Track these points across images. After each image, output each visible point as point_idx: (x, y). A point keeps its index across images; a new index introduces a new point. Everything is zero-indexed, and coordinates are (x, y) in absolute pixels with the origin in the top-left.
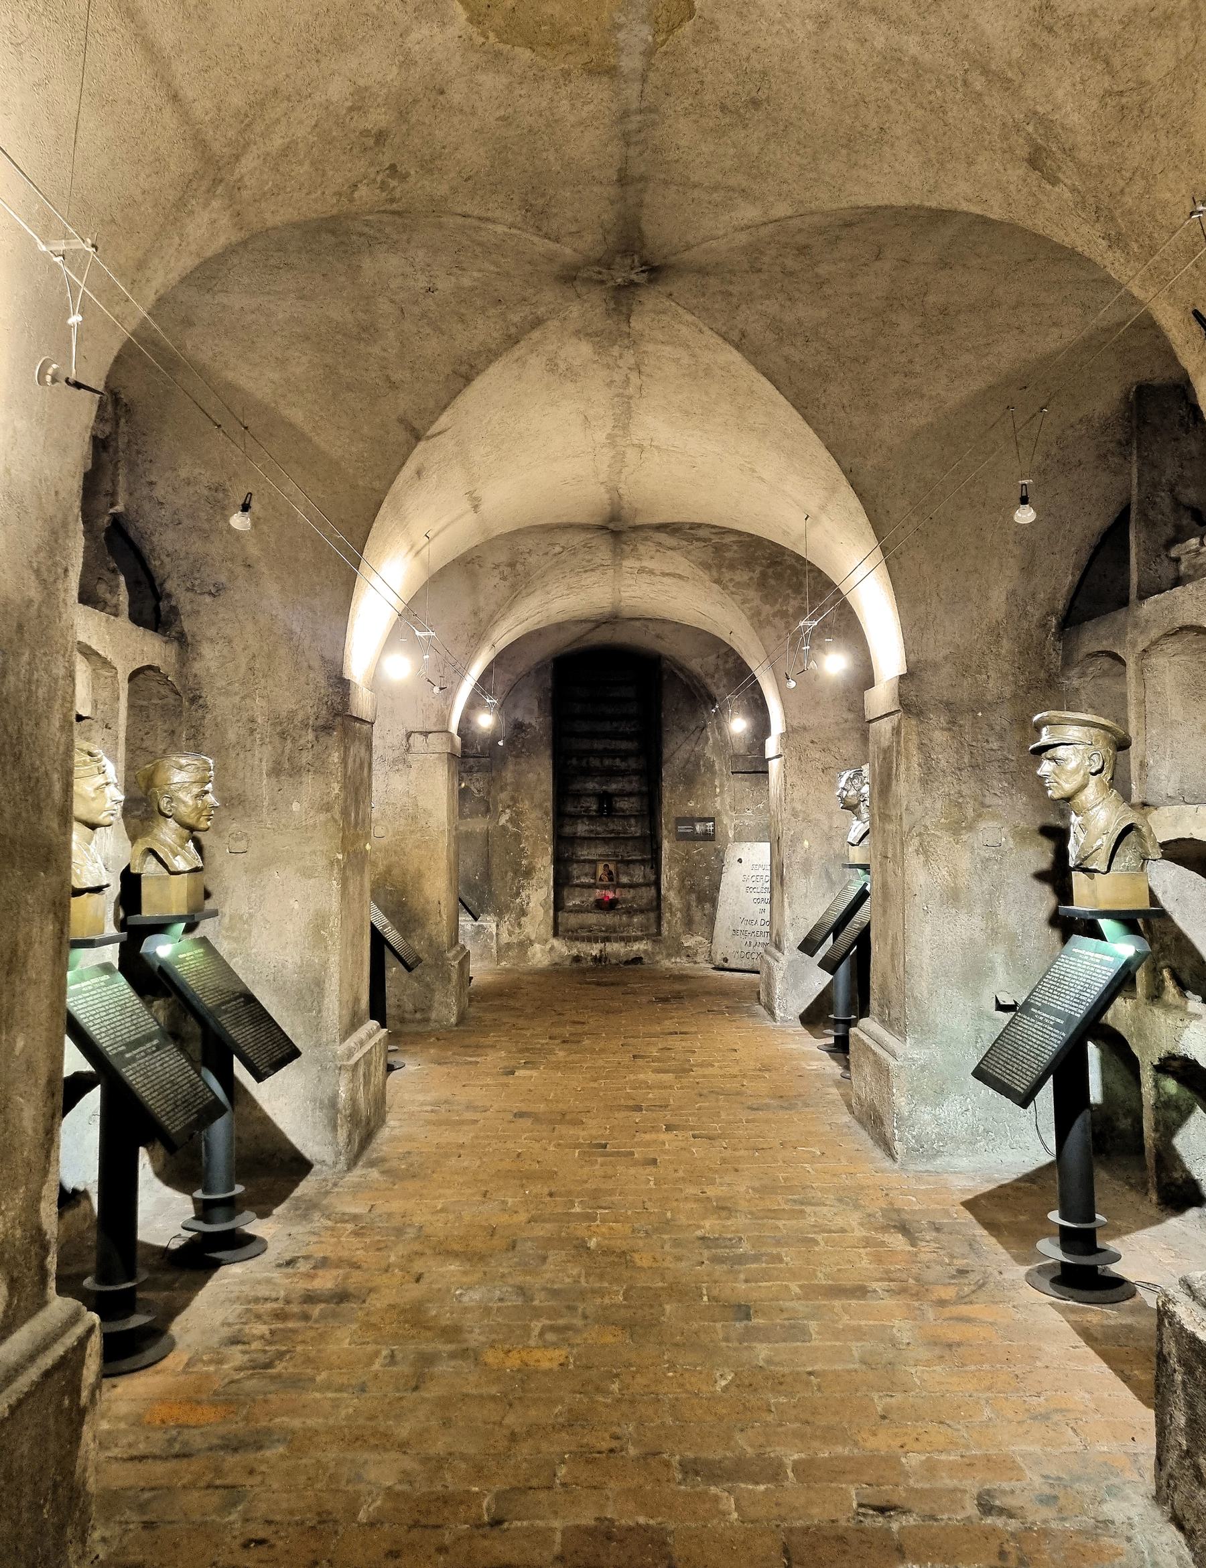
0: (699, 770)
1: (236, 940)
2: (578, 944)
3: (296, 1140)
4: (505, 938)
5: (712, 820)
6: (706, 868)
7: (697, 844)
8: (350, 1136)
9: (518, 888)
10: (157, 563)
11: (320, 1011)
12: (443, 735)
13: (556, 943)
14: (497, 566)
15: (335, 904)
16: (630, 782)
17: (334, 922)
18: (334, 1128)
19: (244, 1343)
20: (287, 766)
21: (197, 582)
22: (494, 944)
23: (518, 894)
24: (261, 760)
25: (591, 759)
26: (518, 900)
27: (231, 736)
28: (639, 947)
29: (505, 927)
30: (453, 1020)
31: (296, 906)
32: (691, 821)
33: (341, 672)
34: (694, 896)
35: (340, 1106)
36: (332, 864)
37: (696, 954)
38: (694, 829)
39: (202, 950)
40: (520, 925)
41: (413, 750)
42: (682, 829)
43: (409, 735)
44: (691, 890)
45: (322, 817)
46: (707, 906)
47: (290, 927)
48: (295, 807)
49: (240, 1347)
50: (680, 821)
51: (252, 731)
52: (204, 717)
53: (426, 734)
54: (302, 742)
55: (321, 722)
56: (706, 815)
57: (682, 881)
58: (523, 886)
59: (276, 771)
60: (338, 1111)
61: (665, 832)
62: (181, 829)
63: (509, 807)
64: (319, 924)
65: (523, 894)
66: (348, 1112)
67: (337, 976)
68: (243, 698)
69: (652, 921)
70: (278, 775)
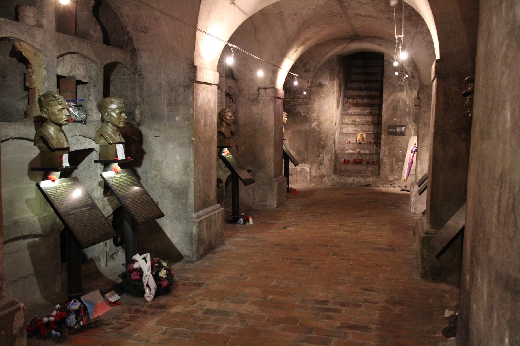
0: (399, 104)
1: (157, 170)
2: (344, 178)
3: (179, 248)
4: (314, 174)
5: (404, 126)
6: (401, 148)
7: (397, 137)
8: (198, 247)
9: (319, 153)
10: (123, 20)
11: (187, 200)
12: (272, 90)
13: (334, 177)
14: (289, 15)
15: (192, 159)
16: (374, 109)
17: (192, 165)
18: (192, 244)
19: (119, 319)
20: (173, 102)
21: (138, 27)
22: (308, 176)
23: (319, 156)
24: (164, 99)
25: (358, 99)
26: (319, 159)
27: (154, 90)
28: (369, 180)
29: (313, 171)
30: (275, 206)
31: (178, 158)
32: (395, 127)
33: (193, 63)
34: (395, 159)
35: (194, 236)
36: (190, 142)
37: (394, 184)
38: (396, 130)
39: (126, 174)
40: (319, 169)
41: (260, 95)
42: (391, 130)
43: (259, 89)
44: (393, 156)
45: (186, 123)
46: (400, 163)
47: (176, 166)
48: (177, 118)
49: (117, 320)
50: (390, 127)
51: (161, 88)
52: (143, 82)
53: (265, 89)
54: (179, 92)
55: (186, 84)
56: (402, 124)
57: (390, 152)
58: (321, 153)
59: (170, 104)
60: (193, 238)
61: (383, 131)
62: (113, 127)
63: (316, 120)
64: (186, 165)
65: (321, 156)
66: (197, 239)
67: (193, 186)
68: (157, 74)
69: (377, 169)
70: (170, 106)
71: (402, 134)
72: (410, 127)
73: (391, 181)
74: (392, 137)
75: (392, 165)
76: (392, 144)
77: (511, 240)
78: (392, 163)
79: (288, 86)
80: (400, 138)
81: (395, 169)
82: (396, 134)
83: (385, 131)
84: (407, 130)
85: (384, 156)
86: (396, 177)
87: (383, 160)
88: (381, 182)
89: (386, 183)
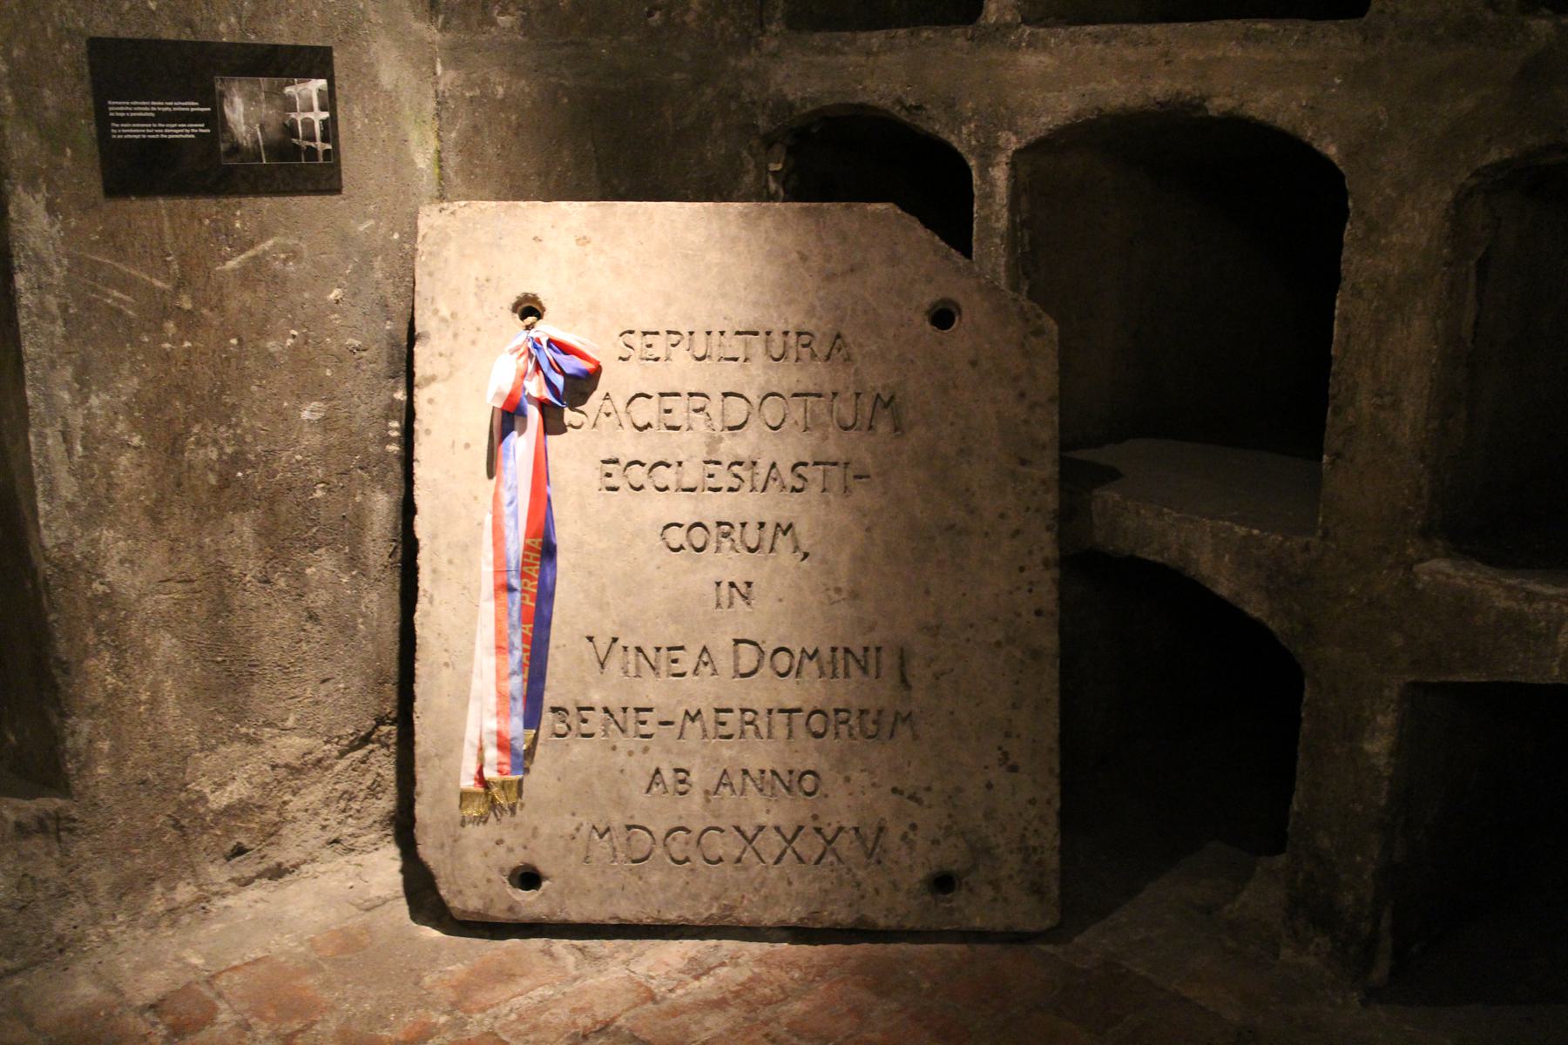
5: (315, 61)
6: (301, 360)
7: (246, 213)
32: (198, 68)
34: (244, 527)
37: (271, 834)
38: (216, 120)
44: (228, 490)
56: (282, 33)
57: (169, 445)
71: (301, 166)
72: (391, 70)
73: (239, 810)
74: (159, 216)
75: (222, 607)
76: (190, 323)
77: (272, 501)
78: (216, 592)
79: (762, 122)
80: (281, 227)
81: (268, 650)
82: (216, 172)
83: (54, 137)
84: (353, 120)
85: (96, 507)
86: (291, 746)
87: (92, 566)
88: (102, 878)
89: (178, 864)
